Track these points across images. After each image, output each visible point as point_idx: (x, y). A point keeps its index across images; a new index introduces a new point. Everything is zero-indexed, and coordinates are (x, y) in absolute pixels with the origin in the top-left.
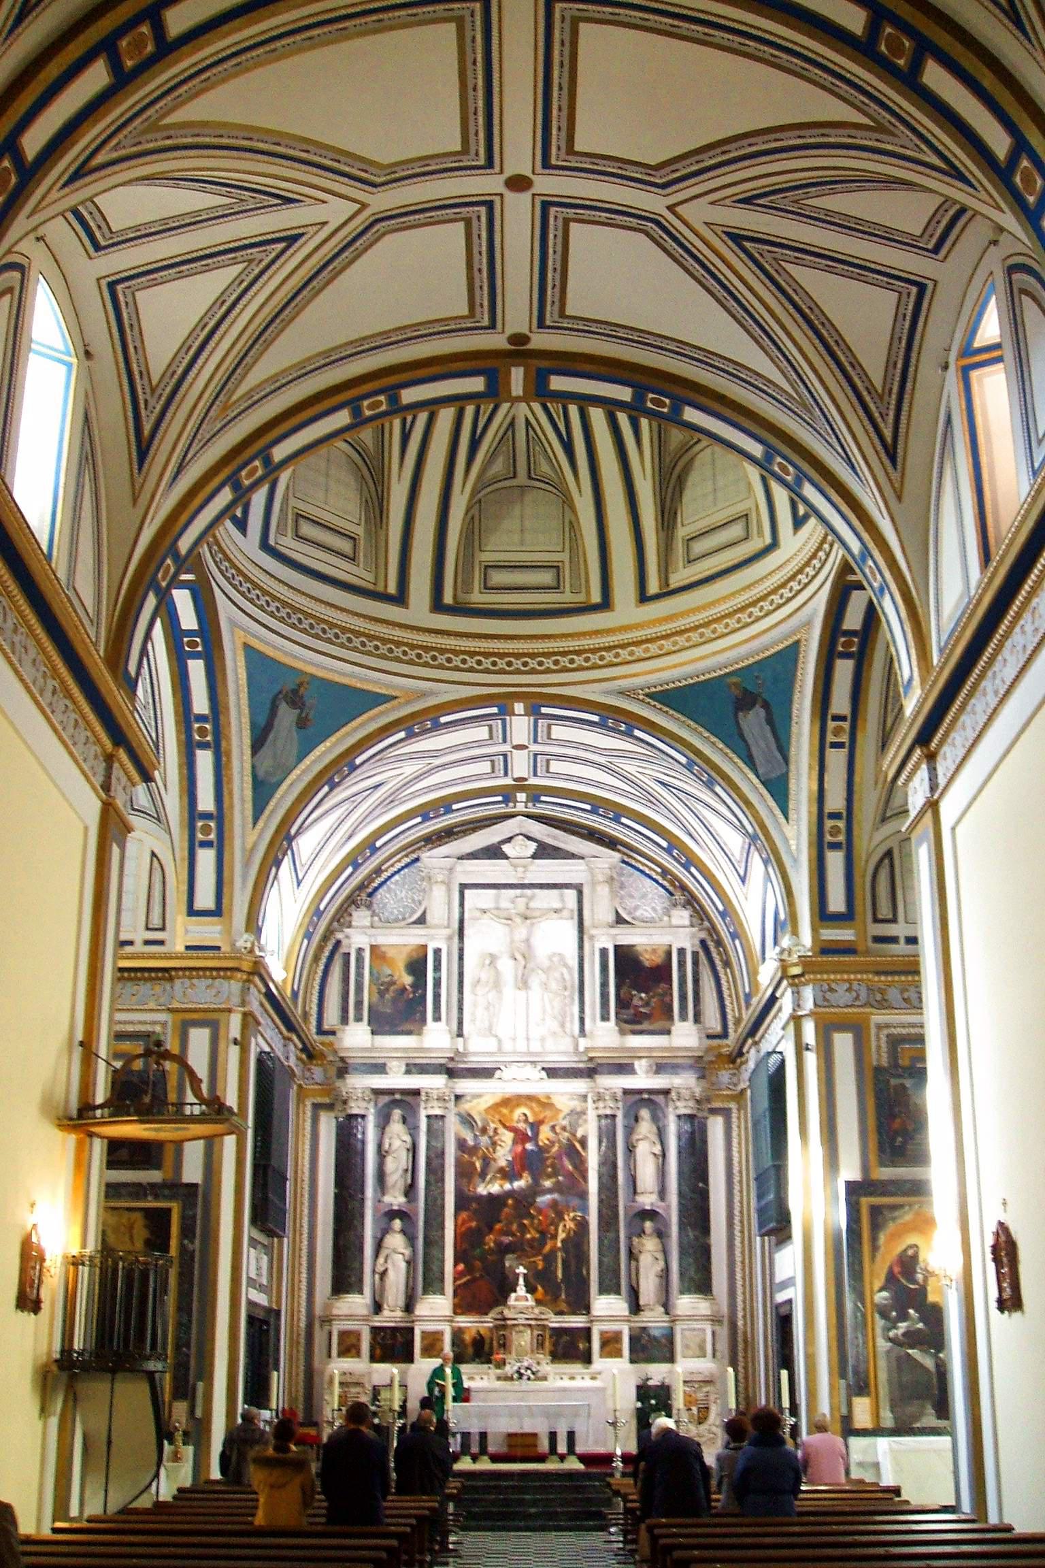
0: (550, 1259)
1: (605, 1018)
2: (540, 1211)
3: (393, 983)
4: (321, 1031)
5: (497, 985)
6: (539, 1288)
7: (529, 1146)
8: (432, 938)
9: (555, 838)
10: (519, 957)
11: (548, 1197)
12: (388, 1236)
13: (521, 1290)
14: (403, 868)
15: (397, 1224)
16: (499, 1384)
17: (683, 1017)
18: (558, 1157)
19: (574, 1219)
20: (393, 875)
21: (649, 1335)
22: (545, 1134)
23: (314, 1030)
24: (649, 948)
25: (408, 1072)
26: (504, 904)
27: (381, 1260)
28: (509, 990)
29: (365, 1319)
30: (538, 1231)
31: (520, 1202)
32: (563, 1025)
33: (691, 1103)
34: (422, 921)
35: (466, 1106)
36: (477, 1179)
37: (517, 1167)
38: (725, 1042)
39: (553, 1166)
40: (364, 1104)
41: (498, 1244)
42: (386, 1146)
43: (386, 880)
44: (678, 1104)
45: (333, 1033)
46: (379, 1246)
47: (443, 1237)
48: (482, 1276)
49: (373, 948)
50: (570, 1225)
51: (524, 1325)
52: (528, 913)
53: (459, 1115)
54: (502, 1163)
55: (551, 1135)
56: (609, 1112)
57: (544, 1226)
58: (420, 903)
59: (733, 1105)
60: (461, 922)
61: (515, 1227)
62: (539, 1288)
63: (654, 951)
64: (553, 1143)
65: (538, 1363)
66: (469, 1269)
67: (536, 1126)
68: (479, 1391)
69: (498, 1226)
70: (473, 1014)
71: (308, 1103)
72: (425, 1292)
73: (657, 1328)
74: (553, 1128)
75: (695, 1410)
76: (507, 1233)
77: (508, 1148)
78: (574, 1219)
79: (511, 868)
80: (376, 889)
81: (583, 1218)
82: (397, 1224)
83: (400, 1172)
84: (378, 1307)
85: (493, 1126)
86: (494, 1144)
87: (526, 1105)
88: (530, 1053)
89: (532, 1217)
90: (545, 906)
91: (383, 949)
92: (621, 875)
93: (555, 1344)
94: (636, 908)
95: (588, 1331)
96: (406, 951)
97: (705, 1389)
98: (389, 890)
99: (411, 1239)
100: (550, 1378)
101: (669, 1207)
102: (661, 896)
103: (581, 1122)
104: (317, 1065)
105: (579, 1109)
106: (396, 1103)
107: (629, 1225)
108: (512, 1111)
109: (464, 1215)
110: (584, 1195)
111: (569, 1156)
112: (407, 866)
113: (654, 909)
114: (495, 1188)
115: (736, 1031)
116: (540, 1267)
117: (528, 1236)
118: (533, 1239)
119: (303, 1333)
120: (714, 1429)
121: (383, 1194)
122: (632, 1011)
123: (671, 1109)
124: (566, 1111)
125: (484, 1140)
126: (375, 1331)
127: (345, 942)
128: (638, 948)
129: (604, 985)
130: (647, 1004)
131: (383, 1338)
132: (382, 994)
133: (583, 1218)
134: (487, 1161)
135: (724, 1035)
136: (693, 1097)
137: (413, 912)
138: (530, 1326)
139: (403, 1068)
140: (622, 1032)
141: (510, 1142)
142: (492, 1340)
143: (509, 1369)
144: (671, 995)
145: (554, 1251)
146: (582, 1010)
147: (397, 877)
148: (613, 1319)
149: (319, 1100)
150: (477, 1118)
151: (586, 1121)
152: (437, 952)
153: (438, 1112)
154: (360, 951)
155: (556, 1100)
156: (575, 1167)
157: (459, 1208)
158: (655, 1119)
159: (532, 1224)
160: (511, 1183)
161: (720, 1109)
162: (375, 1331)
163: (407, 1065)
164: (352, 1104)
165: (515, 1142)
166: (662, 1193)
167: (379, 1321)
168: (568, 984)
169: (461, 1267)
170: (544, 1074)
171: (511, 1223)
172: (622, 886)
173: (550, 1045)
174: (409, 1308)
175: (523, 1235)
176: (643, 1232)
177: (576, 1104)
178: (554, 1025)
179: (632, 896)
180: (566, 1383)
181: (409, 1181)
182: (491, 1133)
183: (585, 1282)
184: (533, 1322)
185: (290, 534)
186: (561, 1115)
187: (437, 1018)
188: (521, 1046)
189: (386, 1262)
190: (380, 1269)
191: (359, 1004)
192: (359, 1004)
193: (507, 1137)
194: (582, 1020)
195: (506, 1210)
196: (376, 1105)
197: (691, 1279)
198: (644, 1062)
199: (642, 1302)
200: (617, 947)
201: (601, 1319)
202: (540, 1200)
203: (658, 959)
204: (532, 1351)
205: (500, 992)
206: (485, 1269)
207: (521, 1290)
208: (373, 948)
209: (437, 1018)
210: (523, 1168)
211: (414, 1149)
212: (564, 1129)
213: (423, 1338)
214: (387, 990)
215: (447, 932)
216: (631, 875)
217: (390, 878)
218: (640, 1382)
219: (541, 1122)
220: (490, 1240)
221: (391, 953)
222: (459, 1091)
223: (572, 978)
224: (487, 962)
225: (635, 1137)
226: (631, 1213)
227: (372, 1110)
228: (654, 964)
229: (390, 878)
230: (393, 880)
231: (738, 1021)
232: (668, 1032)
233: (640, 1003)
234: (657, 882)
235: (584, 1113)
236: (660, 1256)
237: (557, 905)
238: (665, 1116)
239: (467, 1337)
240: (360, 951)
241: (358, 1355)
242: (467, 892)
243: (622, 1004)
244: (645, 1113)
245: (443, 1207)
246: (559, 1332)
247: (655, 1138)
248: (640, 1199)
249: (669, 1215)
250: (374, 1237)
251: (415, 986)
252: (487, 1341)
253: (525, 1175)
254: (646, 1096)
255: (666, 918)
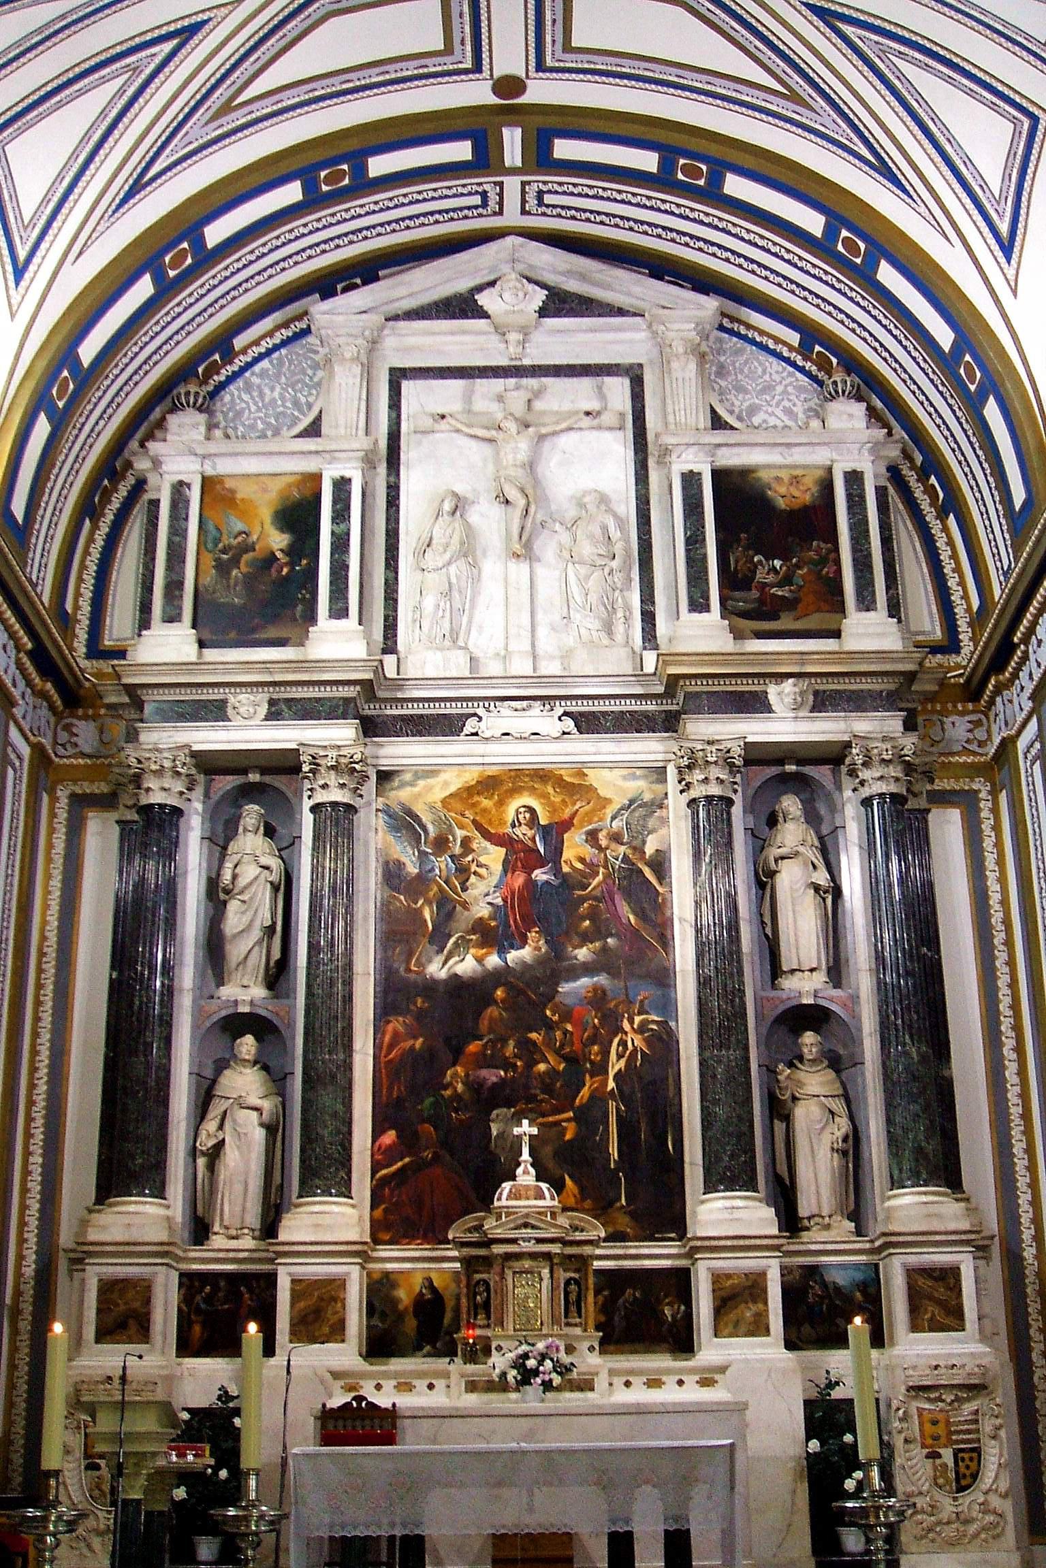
0: (591, 1117)
1: (699, 604)
2: (567, 1015)
3: (248, 548)
4: (96, 651)
5: (468, 550)
6: (568, 1181)
7: (540, 875)
8: (331, 455)
9: (583, 277)
10: (512, 494)
11: (584, 982)
12: (227, 1072)
13: (526, 1176)
14: (276, 348)
15: (247, 1045)
16: (472, 1400)
17: (866, 602)
18: (607, 897)
19: (642, 1029)
20: (257, 360)
21: (824, 1285)
22: (575, 848)
23: (81, 648)
24: (784, 475)
25: (275, 713)
26: (480, 405)
27: (211, 1125)
28: (492, 567)
29: (163, 1252)
30: (565, 1058)
31: (521, 992)
32: (608, 628)
33: (895, 771)
34: (314, 430)
35: (401, 795)
36: (424, 946)
37: (514, 920)
38: (954, 659)
39: (593, 915)
40: (179, 786)
41: (475, 1087)
42: (227, 876)
43: (243, 370)
44: (865, 774)
45: (121, 654)
46: (205, 1097)
47: (348, 1067)
48: (436, 1156)
49: (208, 483)
50: (635, 1041)
51: (533, 1256)
52: (529, 418)
53: (387, 811)
54: (482, 911)
55: (588, 852)
56: (715, 790)
57: (577, 1046)
58: (310, 406)
59: (981, 786)
60: (394, 437)
61: (510, 1048)
62: (568, 1181)
63: (795, 480)
64: (592, 868)
65: (570, 1350)
66: (408, 1142)
67: (555, 833)
68: (418, 1416)
69: (474, 1047)
70: (418, 608)
71: (63, 794)
72: (306, 1189)
73: (842, 1266)
74: (592, 837)
75: (947, 1455)
76: (491, 1063)
77: (494, 880)
78: (642, 1029)
79: (495, 338)
80: (221, 387)
81: (664, 1024)
82: (247, 1045)
83: (256, 934)
84: (200, 1230)
85: (460, 833)
86: (463, 872)
87: (532, 791)
88: (541, 679)
89: (550, 1026)
90: (567, 406)
91: (229, 484)
92: (720, 351)
93: (606, 1309)
94: (753, 410)
95: (680, 1281)
96: (276, 487)
97: (969, 1407)
98: (248, 388)
99: (277, 1080)
100: (601, 1382)
101: (855, 999)
102: (800, 389)
103: (651, 823)
104: (86, 717)
105: (647, 797)
106: (248, 793)
107: (767, 1042)
108: (501, 803)
109: (397, 1024)
110: (664, 978)
111: (628, 895)
112: (284, 343)
113: (789, 412)
114: (466, 966)
115: (974, 639)
116: (568, 1137)
117: (542, 1067)
118: (553, 1073)
119: (29, 1291)
120: (995, 1502)
121: (220, 982)
122: (755, 594)
123: (848, 793)
124: (619, 801)
125: (442, 864)
126: (191, 1282)
127: (152, 479)
128: (764, 475)
129: (694, 541)
130: (787, 580)
131: (209, 1299)
132: (223, 569)
133: (664, 1024)
134: (447, 908)
135: (951, 645)
136: (899, 758)
137: (295, 421)
138: (548, 1256)
139: (263, 710)
140: (738, 635)
141: (497, 868)
142: (458, 1299)
143: (499, 1362)
144: (838, 562)
145: (598, 1098)
146: (648, 597)
147: (265, 364)
148: (742, 1244)
149: (87, 788)
150: (426, 818)
151: (664, 821)
152: (342, 485)
153: (337, 796)
154: (180, 488)
155: (595, 778)
156: (641, 914)
157: (385, 1009)
158: (812, 818)
159: (549, 1042)
160: (502, 952)
161: (953, 792)
162: (191, 1282)
163: (272, 702)
164: (151, 782)
165: (508, 867)
166: (836, 971)
167: (201, 1260)
168: (618, 548)
169: (390, 1137)
170: (569, 724)
171: (504, 1041)
172: (722, 371)
173: (582, 664)
174: (269, 1229)
175: (531, 1064)
176: (795, 1059)
177: (640, 786)
178: (589, 624)
179: (740, 389)
180: (639, 1395)
181: (276, 954)
182: (457, 850)
183: (675, 1165)
184: (555, 1249)
185: (492, 1284)
186: (609, 811)
187: (339, 612)
188: (522, 666)
189: (221, 1127)
190: (206, 1142)
191: (174, 587)
192: (174, 587)
193: (493, 856)
194: (649, 618)
195: (492, 1011)
196: (207, 795)
197: (919, 1151)
198: (788, 685)
199: (803, 1211)
200: (717, 474)
201: (714, 1246)
202: (564, 988)
203: (805, 495)
204: (555, 1320)
205: (474, 565)
206: (445, 1144)
207: (526, 1176)
208: (208, 483)
209: (339, 612)
210: (528, 922)
211: (285, 887)
212: (616, 838)
213: (295, 1297)
214: (235, 561)
215: (363, 443)
216: (738, 352)
217: (249, 365)
218: (814, 1394)
219: (567, 825)
220: (456, 1077)
221: (244, 492)
222: (385, 763)
223: (627, 541)
224: (447, 506)
225: (774, 852)
226: (772, 1014)
227: (199, 806)
228: (796, 505)
229: (249, 365)
230: (257, 368)
231: (978, 619)
232: (837, 634)
233: (771, 578)
234: (793, 364)
235: (659, 804)
236: (838, 1106)
237: (594, 405)
238: (834, 809)
239: (404, 1296)
240: (180, 488)
241: (144, 1334)
242: (407, 386)
243: (732, 581)
244: (791, 804)
245: (349, 999)
246: (614, 1281)
247: (814, 855)
248: (790, 984)
249: (857, 1017)
250: (197, 1075)
251: (293, 552)
252: (450, 1304)
253: (532, 935)
254: (790, 768)
255: (815, 424)
